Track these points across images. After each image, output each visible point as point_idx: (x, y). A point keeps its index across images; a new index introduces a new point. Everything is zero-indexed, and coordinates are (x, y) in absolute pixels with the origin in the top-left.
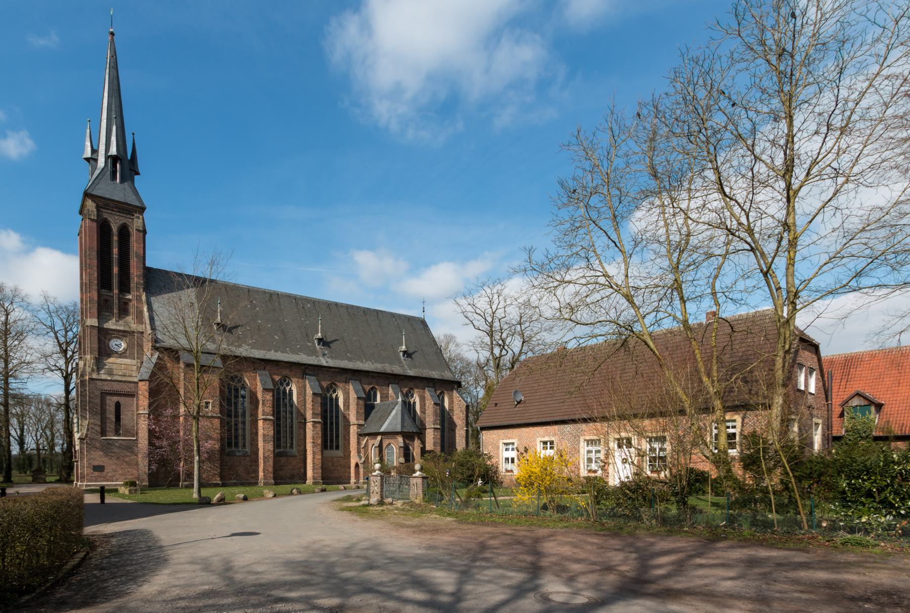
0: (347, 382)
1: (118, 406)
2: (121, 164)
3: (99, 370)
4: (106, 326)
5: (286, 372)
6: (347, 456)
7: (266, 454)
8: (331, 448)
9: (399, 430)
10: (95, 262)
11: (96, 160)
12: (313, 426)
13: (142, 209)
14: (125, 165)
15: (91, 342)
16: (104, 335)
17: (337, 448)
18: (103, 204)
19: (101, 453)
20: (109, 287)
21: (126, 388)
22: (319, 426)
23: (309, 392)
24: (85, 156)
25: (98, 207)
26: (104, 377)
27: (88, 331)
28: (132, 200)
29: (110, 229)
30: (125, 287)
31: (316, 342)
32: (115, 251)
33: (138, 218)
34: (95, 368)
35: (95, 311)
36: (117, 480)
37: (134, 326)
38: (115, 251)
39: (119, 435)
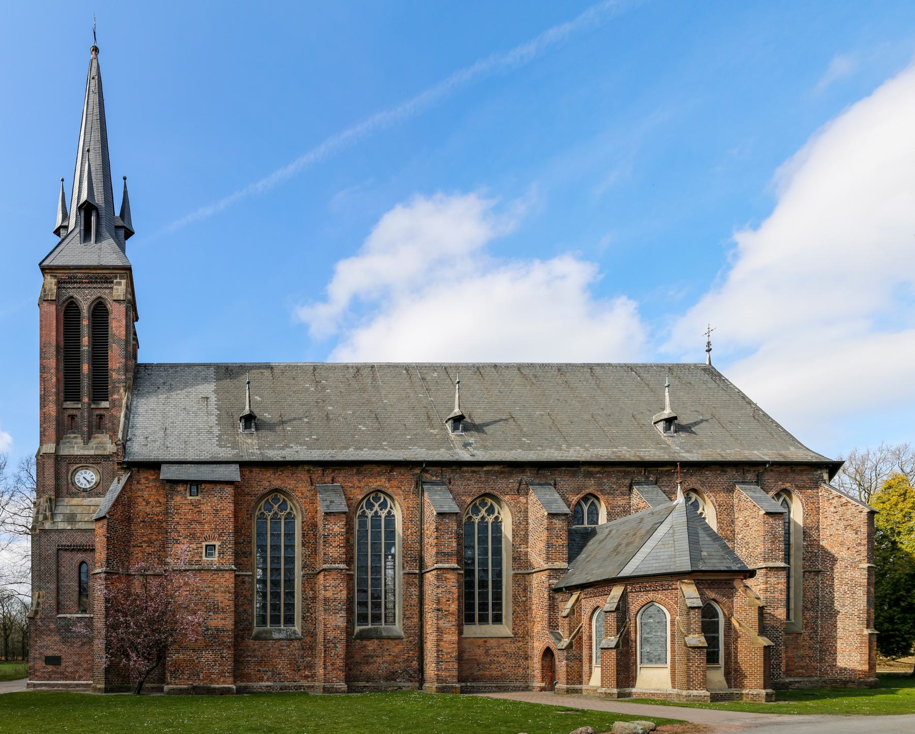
0: (521, 490)
4: (65, 451)
5: (379, 482)
6: (522, 635)
7: (330, 636)
8: (483, 620)
9: (685, 564)
12: (438, 578)
14: (101, 217)
17: (498, 619)
19: (57, 638)
20: (77, 398)
22: (452, 578)
23: (430, 512)
26: (61, 526)
30: (100, 390)
31: (449, 426)
32: (85, 340)
34: (48, 514)
36: (80, 678)
38: (85, 340)
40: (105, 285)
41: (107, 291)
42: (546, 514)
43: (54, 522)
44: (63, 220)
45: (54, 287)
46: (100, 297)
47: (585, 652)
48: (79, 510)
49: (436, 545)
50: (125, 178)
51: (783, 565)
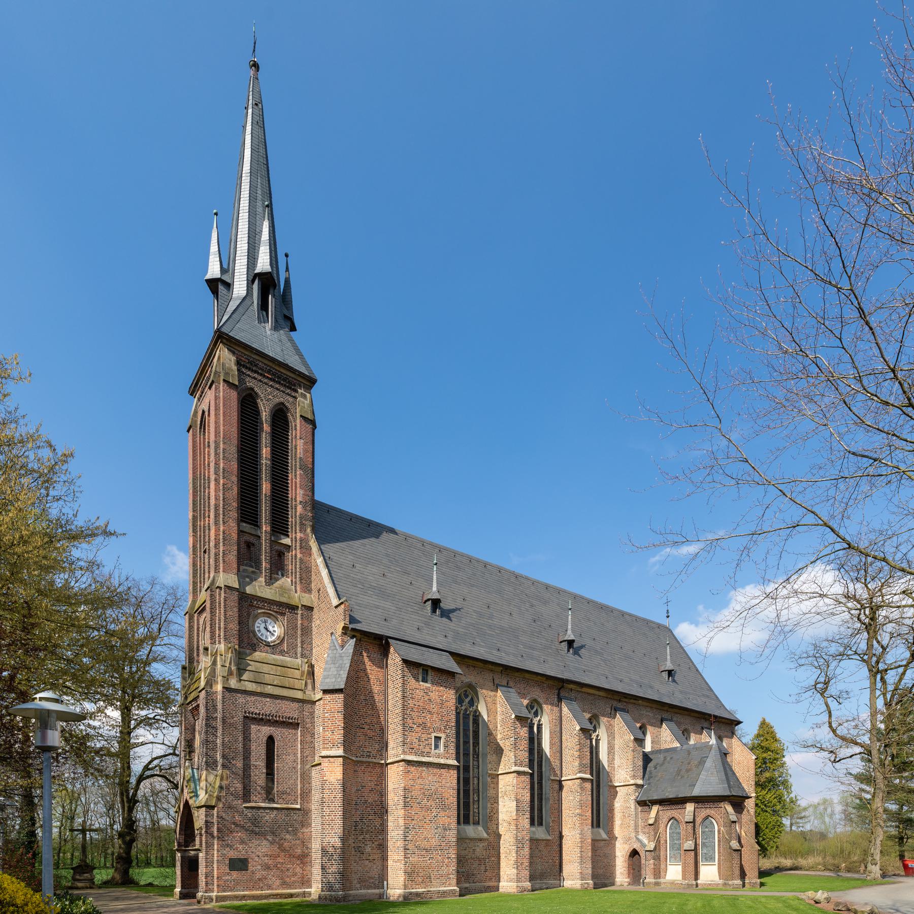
1: (271, 740)
2: (274, 296)
3: (241, 671)
4: (249, 590)
10: (234, 465)
11: (228, 286)
13: (310, 382)
15: (226, 614)
16: (248, 606)
18: (250, 359)
20: (256, 523)
21: (289, 710)
22: (588, 785)
24: (208, 276)
25: (238, 363)
26: (251, 687)
27: (221, 596)
28: (293, 361)
29: (257, 413)
30: (280, 526)
33: (305, 397)
34: (233, 668)
35: (233, 557)
37: (298, 597)
39: (272, 800)
40: (288, 391)
41: (291, 399)
42: (578, 728)
43: (241, 680)
44: (223, 270)
45: (235, 368)
46: (282, 404)
47: (662, 853)
48: (265, 668)
49: (579, 757)
50: (287, 256)
51: (527, 769)
